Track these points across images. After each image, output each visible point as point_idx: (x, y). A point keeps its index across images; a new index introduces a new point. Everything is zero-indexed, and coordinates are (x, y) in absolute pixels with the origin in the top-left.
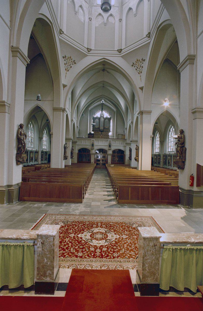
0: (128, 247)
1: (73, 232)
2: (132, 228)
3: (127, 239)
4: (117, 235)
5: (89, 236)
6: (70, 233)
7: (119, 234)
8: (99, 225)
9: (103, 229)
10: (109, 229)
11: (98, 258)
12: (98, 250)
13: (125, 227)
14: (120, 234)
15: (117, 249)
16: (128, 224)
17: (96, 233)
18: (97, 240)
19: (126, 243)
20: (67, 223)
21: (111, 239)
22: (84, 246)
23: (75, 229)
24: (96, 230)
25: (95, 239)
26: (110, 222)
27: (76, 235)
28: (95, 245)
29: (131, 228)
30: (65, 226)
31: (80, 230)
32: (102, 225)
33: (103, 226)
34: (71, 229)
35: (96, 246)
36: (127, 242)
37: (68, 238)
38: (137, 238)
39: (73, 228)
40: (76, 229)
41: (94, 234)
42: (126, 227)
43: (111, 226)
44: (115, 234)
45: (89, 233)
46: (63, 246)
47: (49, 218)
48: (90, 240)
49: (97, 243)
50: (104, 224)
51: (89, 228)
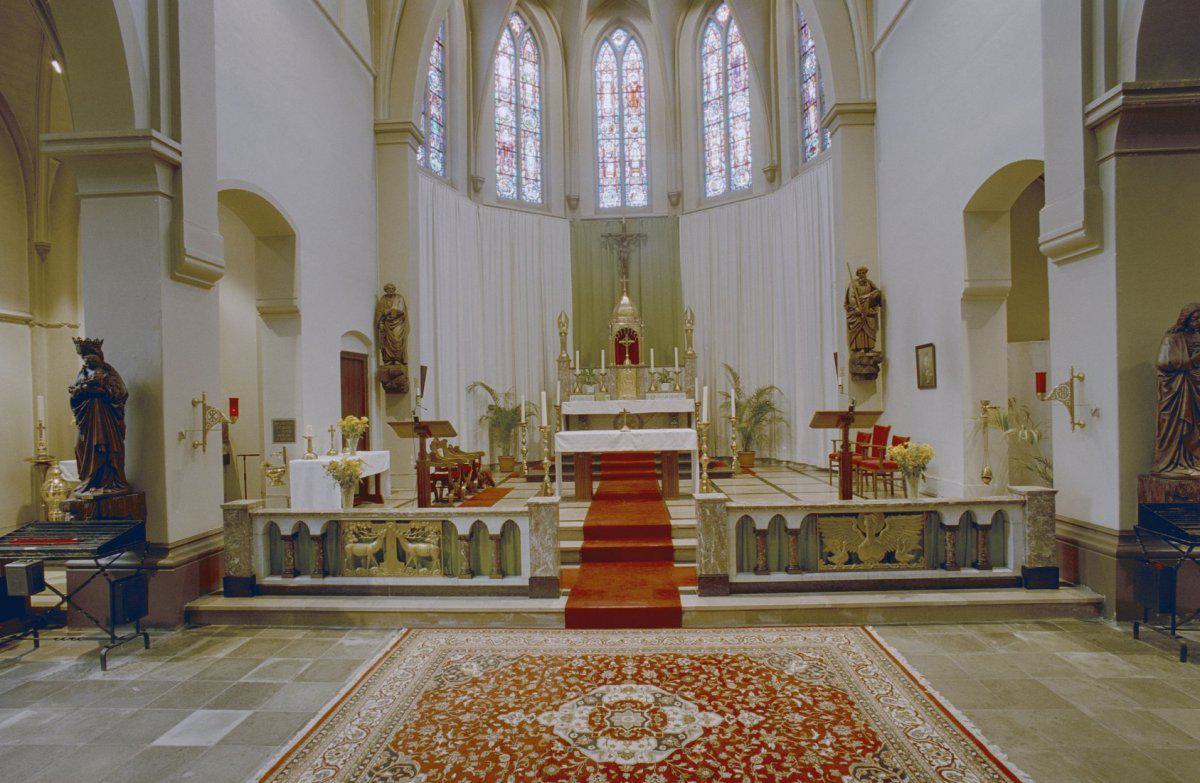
0: (771, 769)
1: (516, 703)
2: (784, 680)
3: (763, 732)
4: (711, 715)
5: (673, 720)
6: (506, 706)
7: (722, 707)
8: (630, 669)
9: (644, 687)
10: (571, 756)
11: (629, 654)
12: (630, 673)
13: (749, 676)
14: (726, 709)
15: (568, 675)
16: (760, 662)
17: (644, 732)
18: (621, 738)
19: (756, 752)
20: (497, 663)
21: (578, 706)
22: (678, 681)
23: (531, 692)
24: (613, 694)
25: (643, 708)
26: (677, 656)
27: (533, 717)
28: (641, 686)
29: (779, 678)
30: (487, 681)
31: (546, 695)
32: (639, 672)
33: (647, 674)
34: (508, 692)
35: (638, 683)
36: (763, 744)
37: (495, 729)
38: (805, 721)
39: (521, 688)
40: (534, 691)
41: (649, 727)
42: (754, 675)
43: (683, 675)
44: (702, 708)
45: (678, 731)
46: (476, 768)
47: (420, 644)
48: (665, 700)
49: (624, 755)
50: (652, 666)
51: (585, 688)
